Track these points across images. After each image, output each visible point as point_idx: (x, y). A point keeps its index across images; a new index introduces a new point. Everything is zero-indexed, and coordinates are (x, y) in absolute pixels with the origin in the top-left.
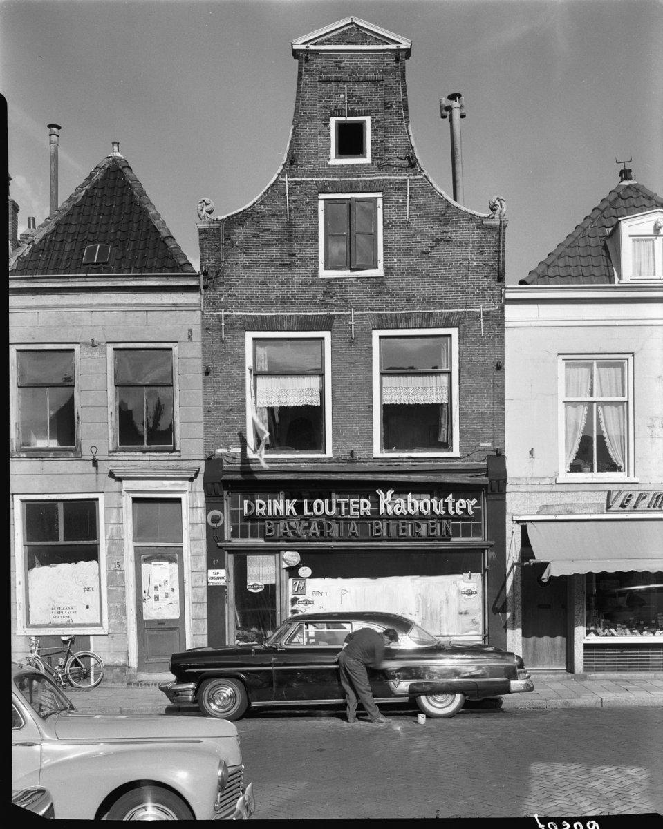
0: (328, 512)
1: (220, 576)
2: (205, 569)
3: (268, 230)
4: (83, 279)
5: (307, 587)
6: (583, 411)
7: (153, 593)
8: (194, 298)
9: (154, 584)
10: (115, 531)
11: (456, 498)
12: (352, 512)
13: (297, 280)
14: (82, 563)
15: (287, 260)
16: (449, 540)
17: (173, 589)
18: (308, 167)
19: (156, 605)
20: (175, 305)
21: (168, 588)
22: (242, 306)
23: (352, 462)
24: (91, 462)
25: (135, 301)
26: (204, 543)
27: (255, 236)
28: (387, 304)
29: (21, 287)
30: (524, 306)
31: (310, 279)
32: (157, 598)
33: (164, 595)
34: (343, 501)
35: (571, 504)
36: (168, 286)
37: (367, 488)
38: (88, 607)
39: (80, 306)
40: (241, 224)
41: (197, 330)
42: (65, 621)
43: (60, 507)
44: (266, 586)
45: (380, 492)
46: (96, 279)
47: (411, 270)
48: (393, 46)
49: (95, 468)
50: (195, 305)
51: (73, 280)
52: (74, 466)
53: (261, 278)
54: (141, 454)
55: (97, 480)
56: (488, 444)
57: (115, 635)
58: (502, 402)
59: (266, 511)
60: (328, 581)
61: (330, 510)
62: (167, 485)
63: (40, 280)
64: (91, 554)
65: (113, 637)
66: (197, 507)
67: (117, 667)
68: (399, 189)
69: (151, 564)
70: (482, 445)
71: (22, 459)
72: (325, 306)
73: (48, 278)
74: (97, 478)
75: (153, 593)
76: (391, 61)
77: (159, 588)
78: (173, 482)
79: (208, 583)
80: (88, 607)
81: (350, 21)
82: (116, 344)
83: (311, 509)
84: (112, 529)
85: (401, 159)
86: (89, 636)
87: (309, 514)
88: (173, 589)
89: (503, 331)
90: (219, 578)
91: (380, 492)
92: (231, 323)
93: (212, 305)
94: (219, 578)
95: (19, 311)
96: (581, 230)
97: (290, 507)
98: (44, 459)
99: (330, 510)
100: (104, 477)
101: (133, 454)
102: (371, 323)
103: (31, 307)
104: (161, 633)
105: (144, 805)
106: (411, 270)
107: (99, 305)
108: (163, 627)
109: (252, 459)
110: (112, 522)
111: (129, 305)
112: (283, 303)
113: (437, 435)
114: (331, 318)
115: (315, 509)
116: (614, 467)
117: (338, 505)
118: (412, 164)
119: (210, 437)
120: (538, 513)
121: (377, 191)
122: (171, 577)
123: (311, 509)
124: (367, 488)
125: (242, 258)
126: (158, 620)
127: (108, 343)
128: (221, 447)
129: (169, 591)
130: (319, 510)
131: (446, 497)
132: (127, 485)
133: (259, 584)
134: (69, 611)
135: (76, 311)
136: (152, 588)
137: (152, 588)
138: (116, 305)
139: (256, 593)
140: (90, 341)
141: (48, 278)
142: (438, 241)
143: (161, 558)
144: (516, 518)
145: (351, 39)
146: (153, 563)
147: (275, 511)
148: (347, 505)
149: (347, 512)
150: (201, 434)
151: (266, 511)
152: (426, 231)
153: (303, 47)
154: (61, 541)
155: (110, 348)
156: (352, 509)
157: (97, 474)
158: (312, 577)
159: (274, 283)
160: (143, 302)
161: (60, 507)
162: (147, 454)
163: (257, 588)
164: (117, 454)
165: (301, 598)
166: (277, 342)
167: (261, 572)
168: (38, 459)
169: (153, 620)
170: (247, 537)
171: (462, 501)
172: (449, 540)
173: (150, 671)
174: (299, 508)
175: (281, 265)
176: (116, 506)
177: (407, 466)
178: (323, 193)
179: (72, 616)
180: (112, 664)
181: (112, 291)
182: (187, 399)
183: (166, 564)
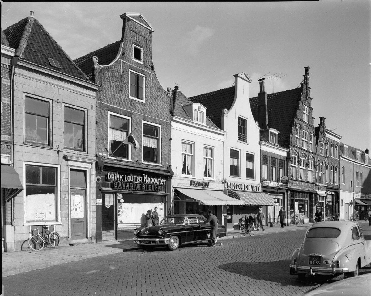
0: (131, 181)
1: (100, 201)
2: (95, 198)
3: (115, 76)
4: (60, 74)
5: (123, 206)
6: (184, 156)
7: (75, 207)
8: (94, 94)
9: (75, 204)
10: (65, 182)
11: (161, 179)
12: (137, 181)
13: (123, 97)
14: (48, 194)
15: (121, 89)
16: (158, 192)
17: (82, 206)
18: (127, 58)
19: (76, 212)
20: (88, 95)
21: (80, 206)
22: (107, 101)
23: (136, 164)
24: (56, 152)
25: (74, 89)
26: (95, 189)
27: (112, 77)
28: (146, 113)
29: (34, 69)
30: (178, 124)
31: (126, 98)
32: (76, 209)
33: (79, 208)
34: (135, 177)
35: (184, 183)
36: (88, 87)
37: (141, 173)
38: (50, 213)
39: (55, 85)
40: (108, 71)
41: (94, 106)
42: (41, 219)
43: (41, 169)
44: (111, 205)
45: (144, 175)
46: (65, 76)
47: (152, 103)
48: (150, 29)
49: (58, 154)
50: (94, 97)
51: (56, 73)
52: (50, 152)
53: (113, 93)
54: (74, 151)
55: (58, 160)
56: (168, 163)
57: (64, 225)
58: (170, 151)
59: (114, 178)
60: (128, 204)
61: (132, 180)
62: (84, 165)
63: (45, 69)
64: (52, 190)
65: (63, 225)
66: (93, 175)
67: (65, 238)
68: (149, 76)
69: (74, 196)
70: (166, 163)
71: (29, 146)
72: (131, 109)
73: (46, 69)
74: (58, 158)
75: (75, 207)
76: (148, 33)
77: (77, 205)
78: (86, 164)
79: (96, 204)
80: (50, 213)
81: (140, 14)
82: (66, 104)
83: (127, 179)
84: (64, 180)
85: (150, 66)
86: (54, 225)
87: (126, 180)
88: (82, 206)
89: (171, 129)
90: (100, 202)
91: (144, 175)
92: (105, 106)
93: (98, 98)
94: (100, 202)
95: (29, 78)
96: (31, 38)
97: (121, 178)
98: (38, 147)
99: (132, 180)
100: (61, 158)
101: (71, 150)
102: (142, 119)
103: (35, 79)
104: (77, 223)
105: (191, 224)
106: (152, 103)
107: (62, 87)
108: (78, 221)
109: (69, 159)
110: (64, 177)
111: (73, 90)
112: (119, 104)
113: (153, 158)
114: (132, 113)
115: (128, 179)
116: (189, 174)
117: (134, 178)
118: (153, 68)
119: (97, 149)
120: (177, 185)
121: (144, 74)
122: (81, 201)
123: (127, 179)
124: (141, 173)
125: (107, 83)
126: (76, 218)
127: (63, 103)
128: (100, 153)
129: (80, 207)
130: (129, 179)
131: (159, 178)
132: (70, 163)
133: (109, 205)
134: (42, 214)
135: (52, 86)
136: (75, 205)
137: (75, 205)
138: (68, 88)
139: (108, 208)
140: (57, 100)
141: (46, 69)
142: (158, 96)
143: (78, 194)
144: (173, 186)
145: (139, 20)
146: (75, 195)
147: (117, 178)
148: (136, 178)
149: (136, 181)
150: (95, 147)
151: (114, 178)
152: (156, 93)
153: (128, 16)
154: (41, 184)
155: (64, 105)
156: (137, 180)
157: (58, 157)
158: (124, 203)
159: (117, 96)
160: (77, 90)
161: (41, 169)
162: (76, 151)
163: (108, 206)
164: (65, 149)
165: (121, 210)
166: (115, 117)
167: (109, 201)
168: (36, 147)
169: (75, 218)
170: (106, 187)
171: (162, 180)
172: (158, 192)
173: (77, 239)
174: (123, 178)
175: (119, 90)
176: (65, 171)
177: (150, 167)
178: (131, 69)
179: (44, 217)
180: (62, 237)
181: (68, 82)
182: (90, 132)
183: (80, 196)
